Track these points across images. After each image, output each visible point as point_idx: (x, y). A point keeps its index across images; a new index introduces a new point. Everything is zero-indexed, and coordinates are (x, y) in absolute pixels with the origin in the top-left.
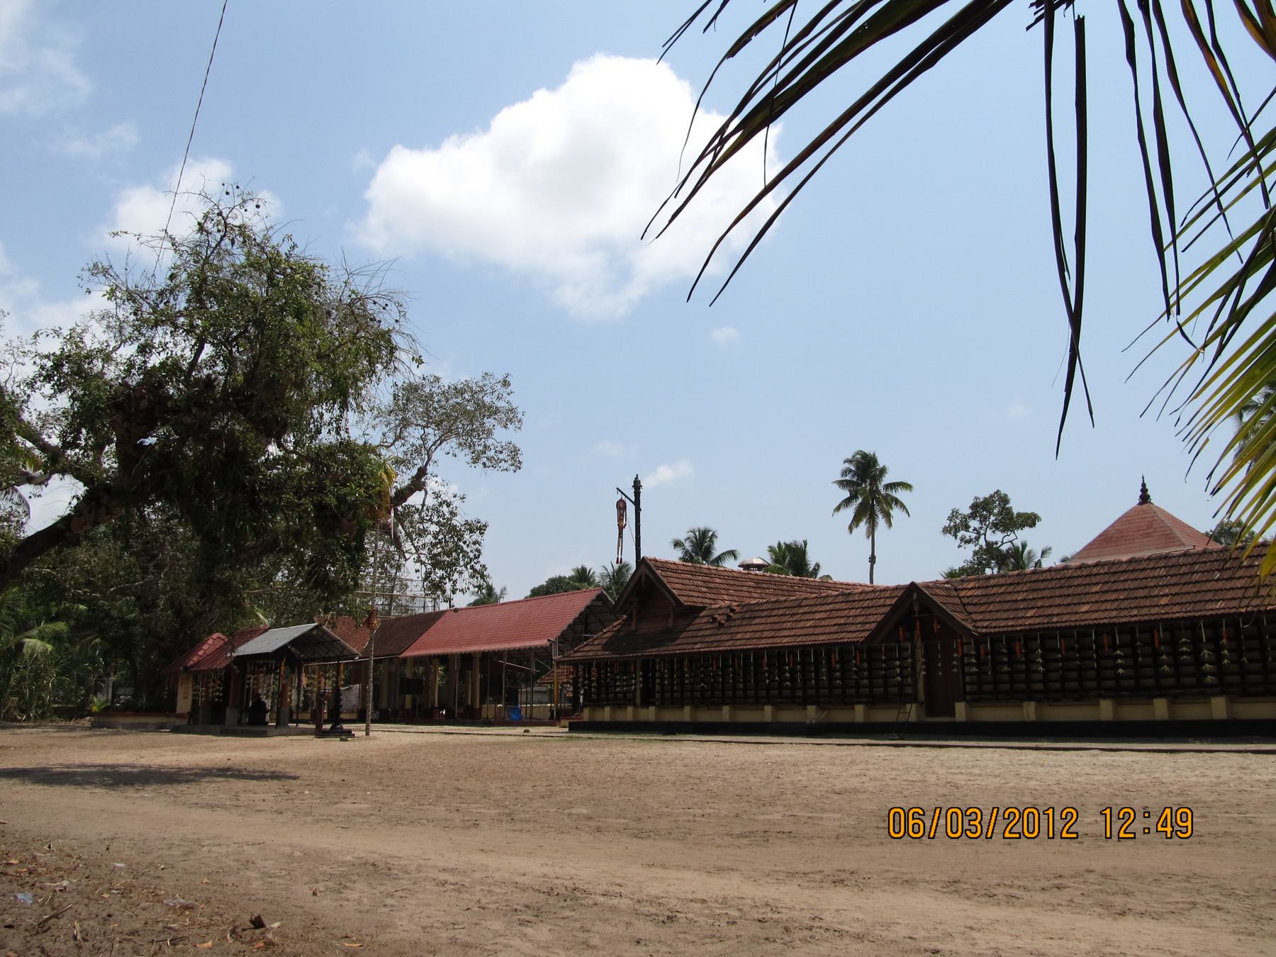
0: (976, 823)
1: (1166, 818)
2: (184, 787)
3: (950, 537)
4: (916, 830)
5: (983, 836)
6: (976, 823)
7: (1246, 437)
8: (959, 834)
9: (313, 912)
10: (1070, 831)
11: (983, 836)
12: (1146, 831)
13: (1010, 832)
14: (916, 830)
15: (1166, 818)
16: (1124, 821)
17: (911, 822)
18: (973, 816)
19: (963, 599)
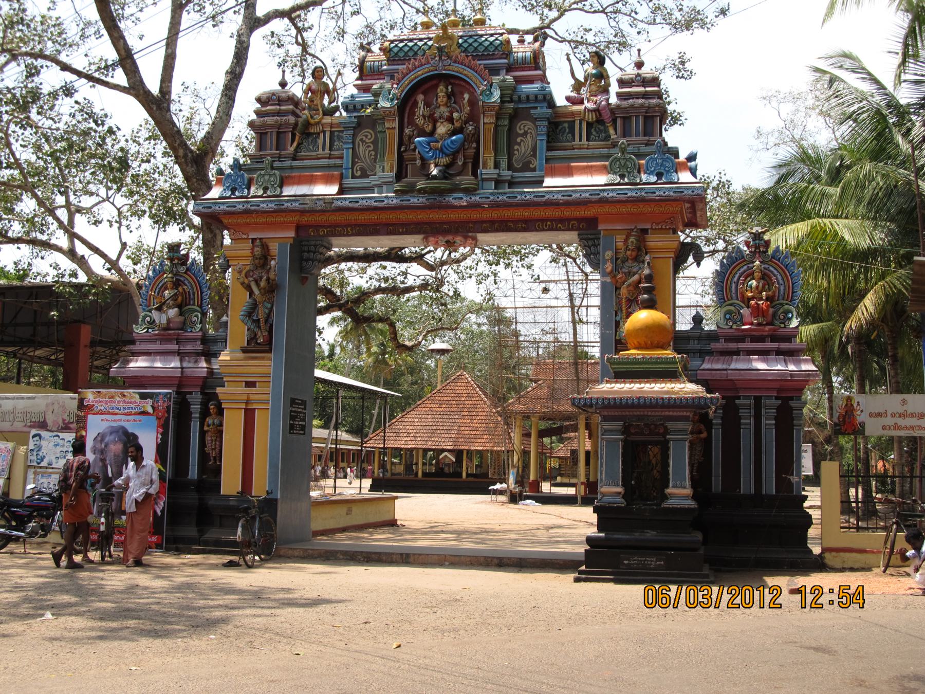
0: (708, 597)
1: (859, 593)
2: (123, 642)
3: (711, 31)
4: (664, 602)
5: (671, 606)
6: (708, 597)
7: (119, 349)
8: (695, 605)
9: (628, 38)
10: (818, 602)
11: (671, 606)
12: (831, 602)
13: (774, 604)
14: (664, 602)
15: (859, 593)
16: (772, 595)
17: (661, 596)
18: (706, 592)
19: (583, 304)
